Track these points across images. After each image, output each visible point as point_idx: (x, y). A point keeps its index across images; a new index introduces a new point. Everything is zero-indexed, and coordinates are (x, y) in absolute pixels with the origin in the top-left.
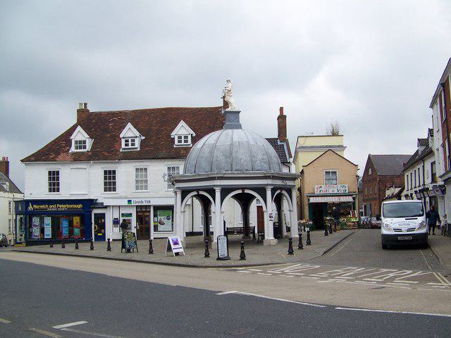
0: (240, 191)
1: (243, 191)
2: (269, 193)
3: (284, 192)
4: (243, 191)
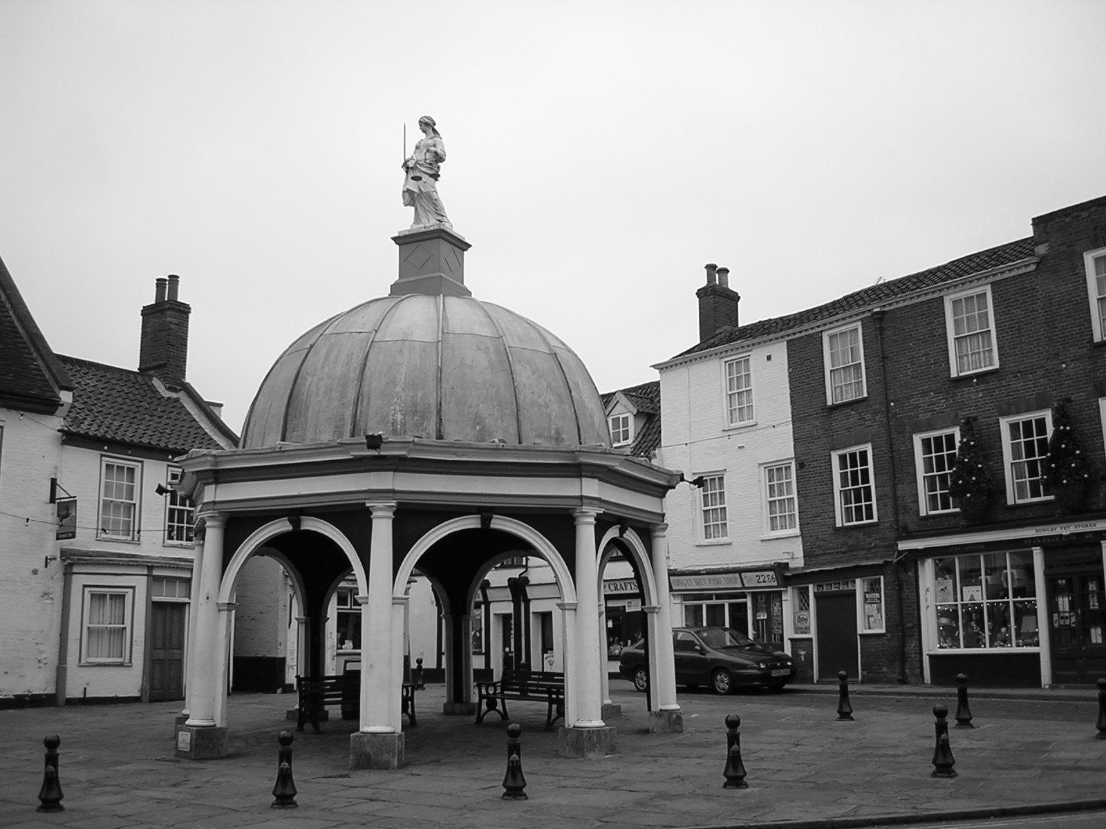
0: (470, 523)
1: (486, 521)
2: (586, 533)
3: (631, 537)
4: (486, 521)
